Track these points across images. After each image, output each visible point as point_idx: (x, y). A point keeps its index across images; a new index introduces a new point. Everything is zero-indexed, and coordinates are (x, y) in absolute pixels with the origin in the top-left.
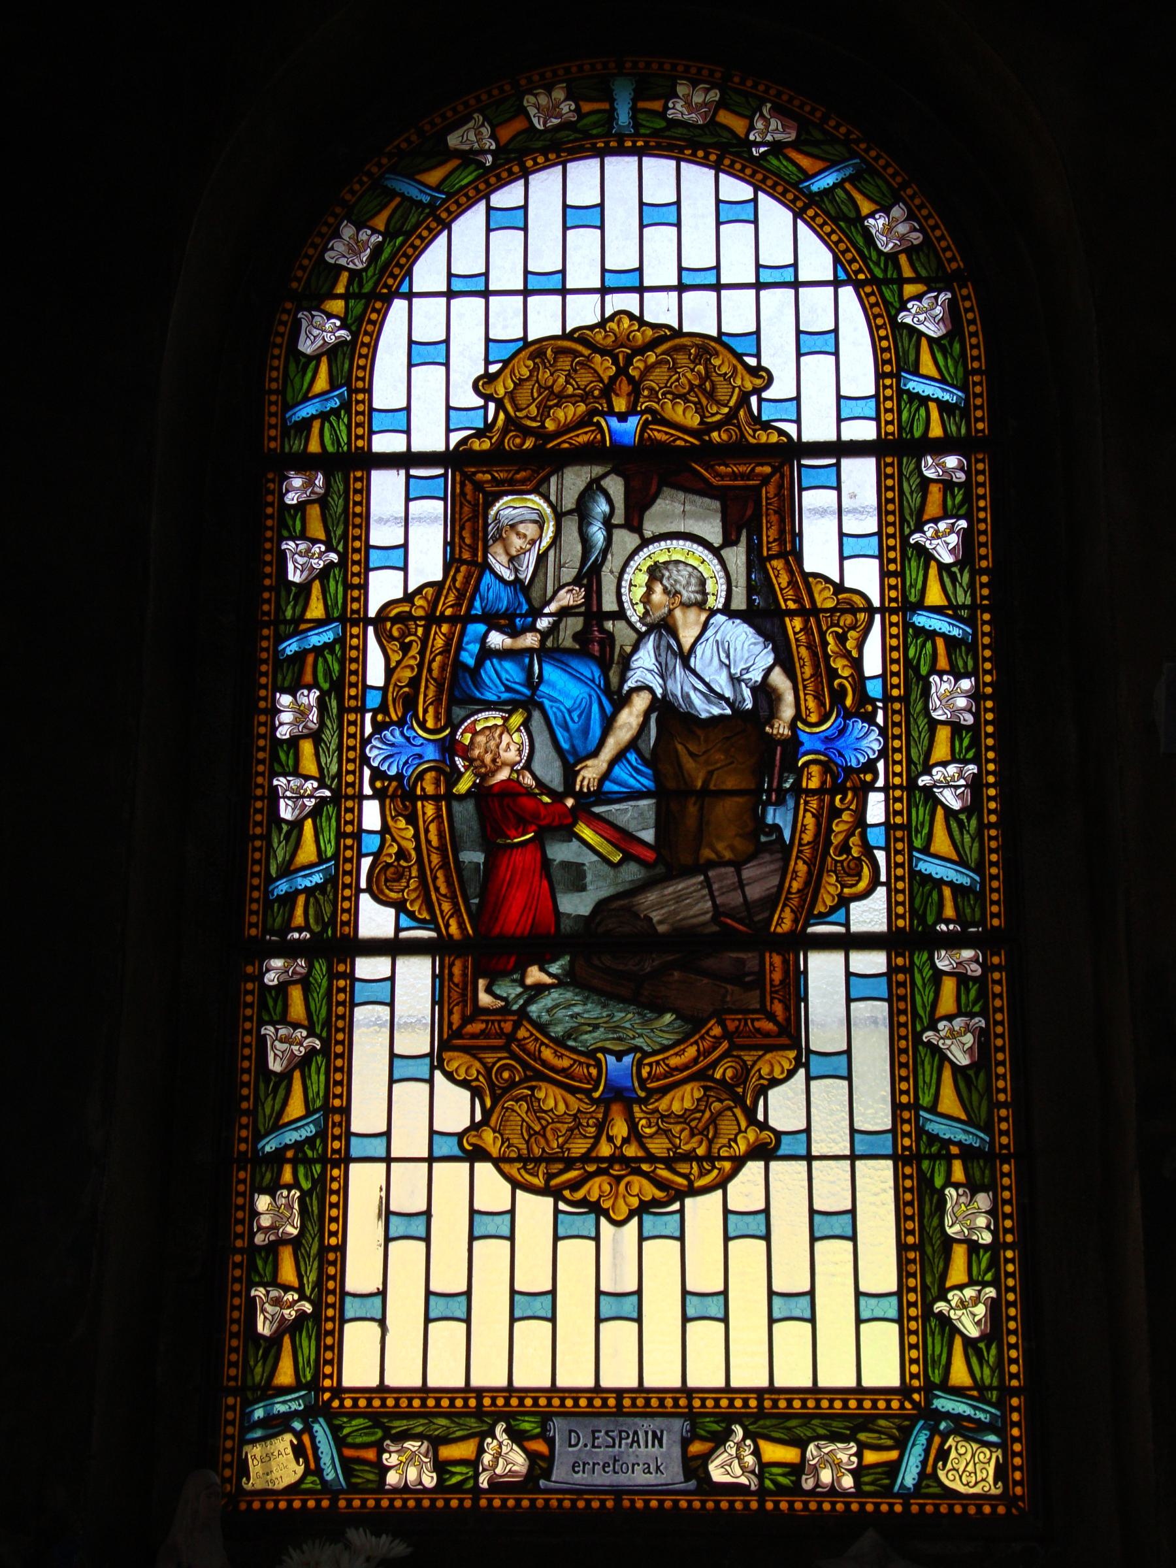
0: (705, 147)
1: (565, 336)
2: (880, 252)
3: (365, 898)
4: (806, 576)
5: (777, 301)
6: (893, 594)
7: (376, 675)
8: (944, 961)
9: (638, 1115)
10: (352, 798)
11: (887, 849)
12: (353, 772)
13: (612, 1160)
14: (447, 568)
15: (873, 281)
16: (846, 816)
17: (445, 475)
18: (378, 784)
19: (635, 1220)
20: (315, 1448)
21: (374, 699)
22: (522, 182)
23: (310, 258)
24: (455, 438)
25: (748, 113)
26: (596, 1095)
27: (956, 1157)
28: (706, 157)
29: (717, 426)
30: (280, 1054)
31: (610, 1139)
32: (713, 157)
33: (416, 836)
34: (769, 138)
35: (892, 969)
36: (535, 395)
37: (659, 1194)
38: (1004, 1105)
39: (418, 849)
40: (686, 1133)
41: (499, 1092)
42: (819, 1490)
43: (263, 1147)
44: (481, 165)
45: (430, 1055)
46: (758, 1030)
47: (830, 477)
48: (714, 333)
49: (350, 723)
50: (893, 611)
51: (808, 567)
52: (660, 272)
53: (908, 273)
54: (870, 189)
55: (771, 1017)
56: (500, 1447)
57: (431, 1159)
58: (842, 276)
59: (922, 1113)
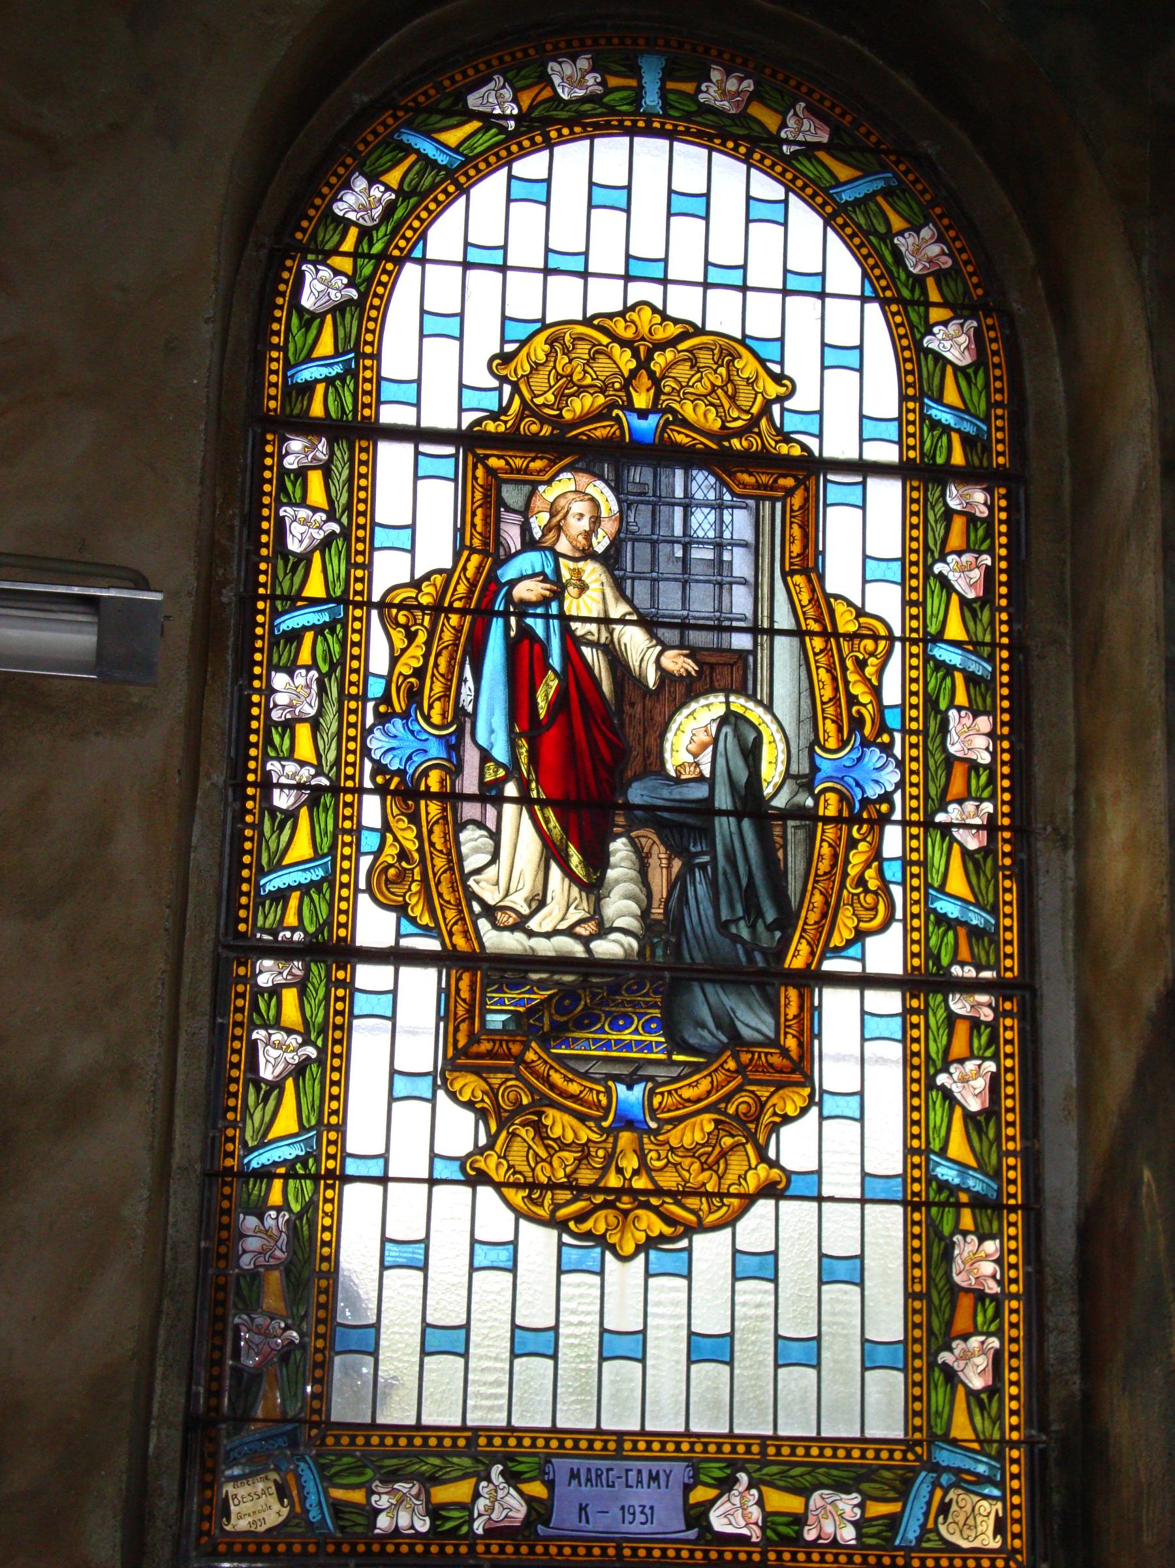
0: (736, 139)
1: (587, 321)
2: (909, 274)
3: (364, 899)
4: (827, 596)
5: (803, 309)
6: (914, 624)
7: (379, 662)
8: (959, 1005)
9: (648, 1146)
10: (351, 791)
11: (903, 883)
12: (353, 765)
13: (619, 1192)
14: (457, 555)
15: (899, 300)
16: (862, 846)
18: (380, 780)
19: (642, 1256)
20: (301, 1488)
21: (376, 689)
22: (546, 153)
23: (317, 208)
24: (468, 418)
25: (781, 109)
26: (605, 1124)
27: (965, 1205)
28: (735, 149)
29: (740, 433)
30: (273, 1061)
31: (620, 1171)
32: (742, 150)
33: (419, 836)
34: (800, 138)
35: (907, 1012)
36: (552, 383)
37: (668, 1230)
38: (1013, 1154)
39: (420, 850)
40: (696, 1166)
41: (505, 1115)
42: (821, 1541)
43: (249, 1162)
44: (503, 130)
45: (433, 1074)
46: (771, 1065)
47: (855, 495)
48: (739, 337)
49: (350, 712)
50: (914, 642)
51: (830, 589)
52: (685, 265)
53: (934, 296)
54: (902, 206)
55: (785, 1052)
56: (496, 1492)
57: (432, 1182)
58: (869, 292)
59: (933, 1157)
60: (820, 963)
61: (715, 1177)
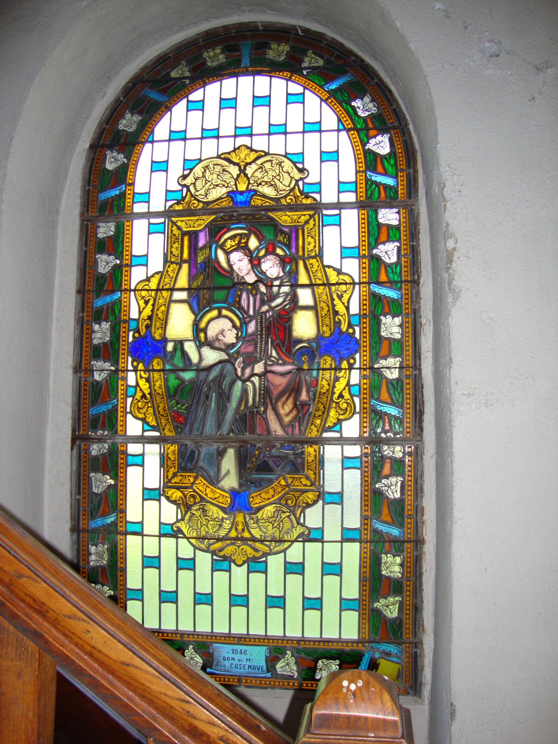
3: (129, 416)
4: (324, 267)
5: (312, 138)
13: (236, 539)
17: (164, 223)
19: (246, 564)
22: (202, 89)
24: (169, 204)
33: (150, 388)
48: (284, 154)
52: (261, 127)
58: (341, 127)
60: (321, 434)
61: (277, 530)
